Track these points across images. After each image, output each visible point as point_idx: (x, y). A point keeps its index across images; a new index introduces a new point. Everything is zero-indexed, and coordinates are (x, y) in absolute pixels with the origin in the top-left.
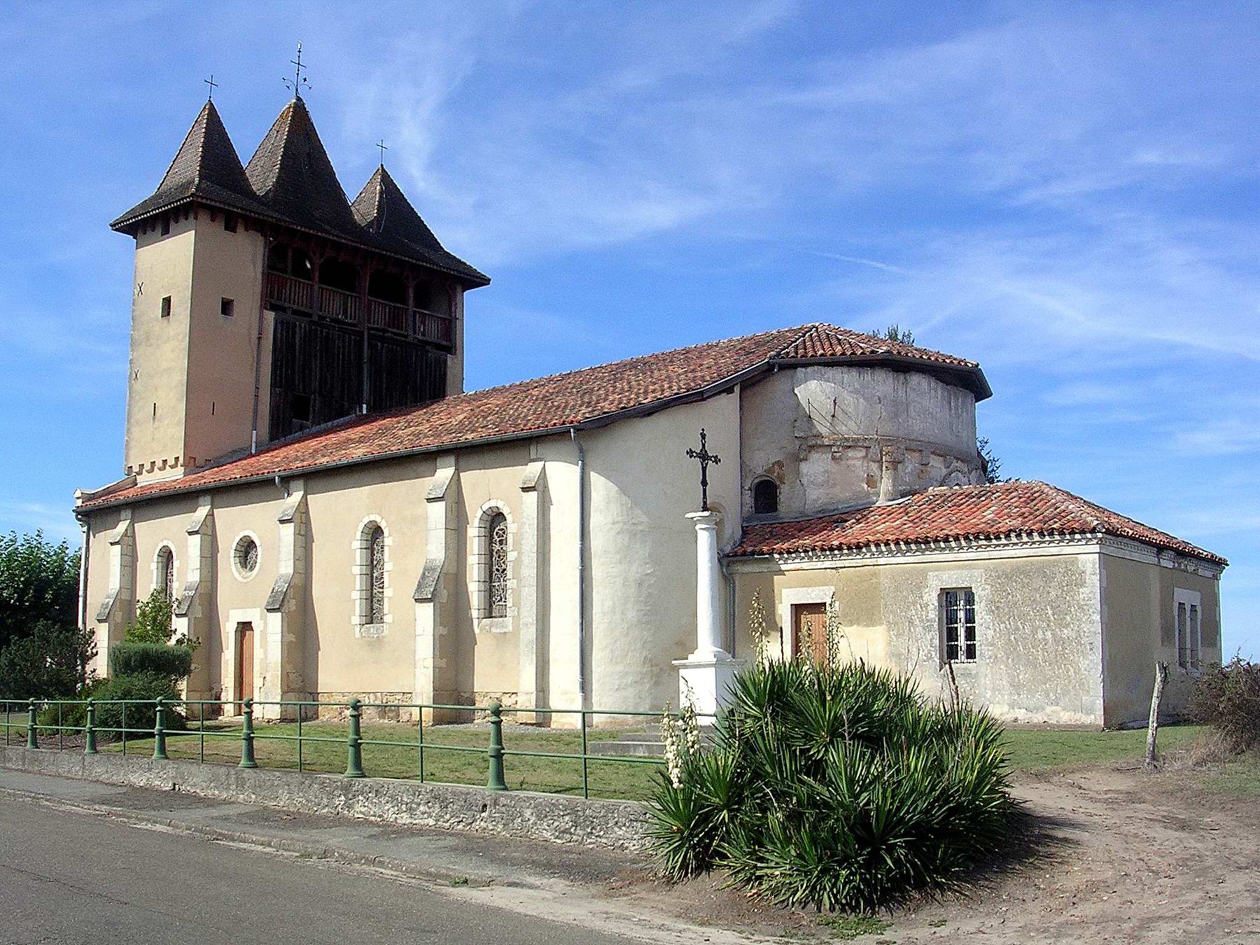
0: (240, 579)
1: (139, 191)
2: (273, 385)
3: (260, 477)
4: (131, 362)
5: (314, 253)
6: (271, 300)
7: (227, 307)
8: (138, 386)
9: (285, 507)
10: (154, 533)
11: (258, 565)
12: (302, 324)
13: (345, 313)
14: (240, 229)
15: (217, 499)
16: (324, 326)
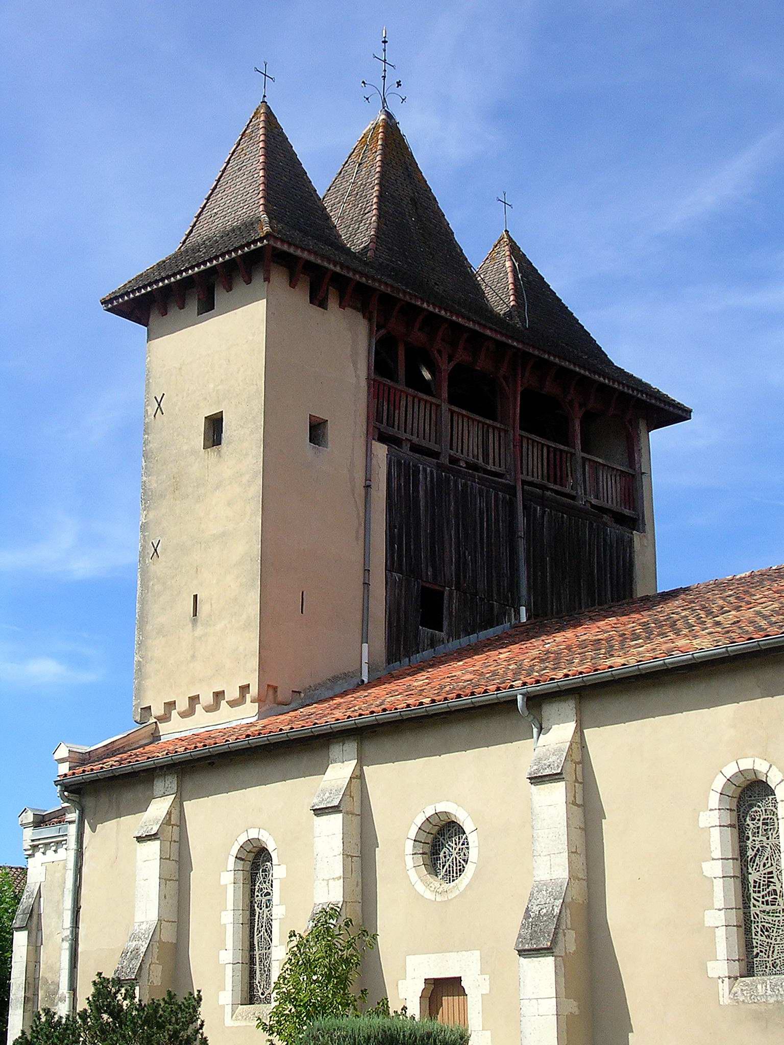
0: (429, 895)
1: (146, 245)
2: (389, 569)
3: (479, 699)
4: (144, 527)
5: (439, 352)
6: (381, 428)
7: (317, 431)
8: (158, 568)
9: (540, 751)
10: (222, 819)
11: (470, 869)
12: (427, 468)
13: (486, 456)
14: (333, 304)
15: (371, 748)
16: (457, 473)
